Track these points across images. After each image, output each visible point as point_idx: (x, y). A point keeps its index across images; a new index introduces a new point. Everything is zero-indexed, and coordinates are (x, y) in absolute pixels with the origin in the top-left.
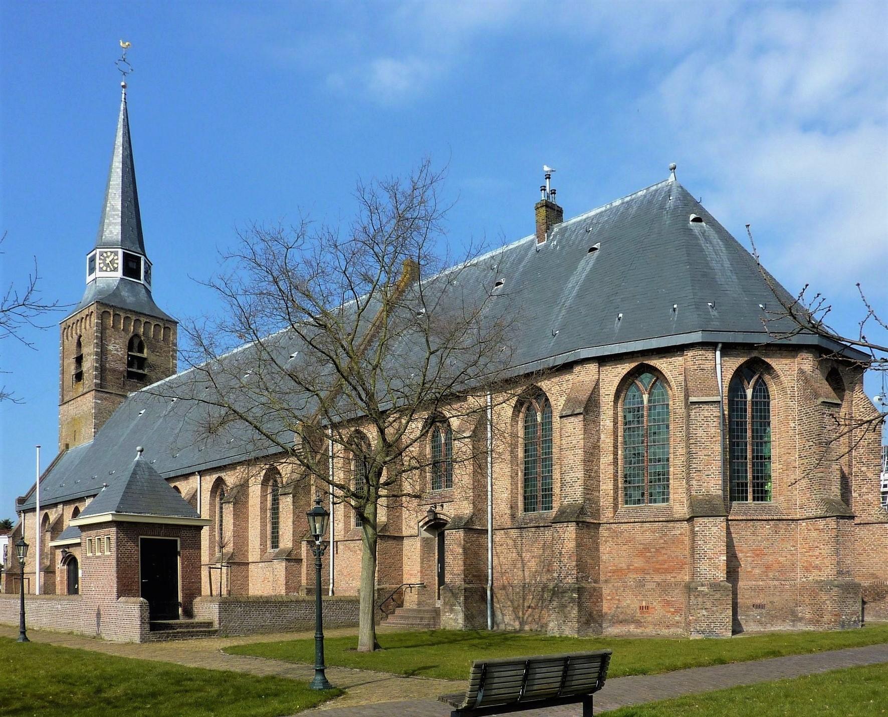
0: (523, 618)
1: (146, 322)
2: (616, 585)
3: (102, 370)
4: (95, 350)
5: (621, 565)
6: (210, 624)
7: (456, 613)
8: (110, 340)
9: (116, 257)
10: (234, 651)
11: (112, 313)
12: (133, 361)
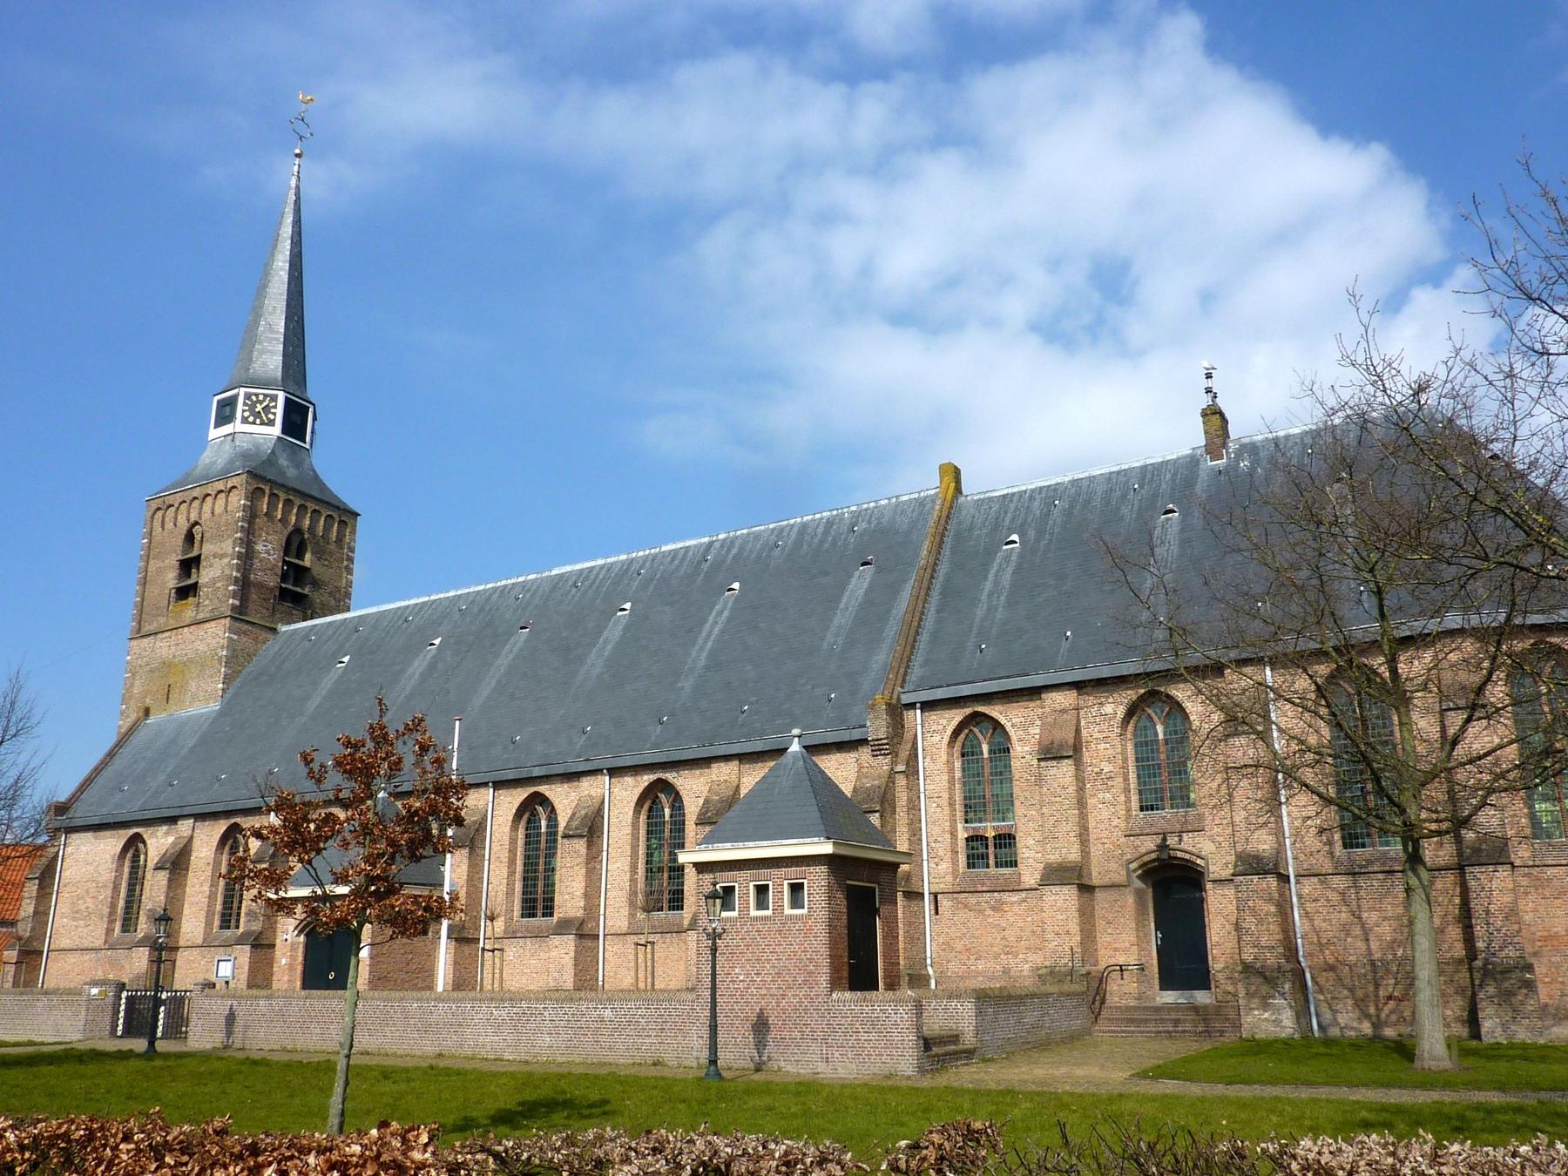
0: (1378, 1016)
1: (315, 511)
2: (1553, 959)
3: (245, 585)
4: (237, 549)
5: (1555, 929)
6: (955, 1038)
7: (1278, 1010)
8: (260, 536)
9: (273, 404)
11: (267, 492)
12: (295, 573)
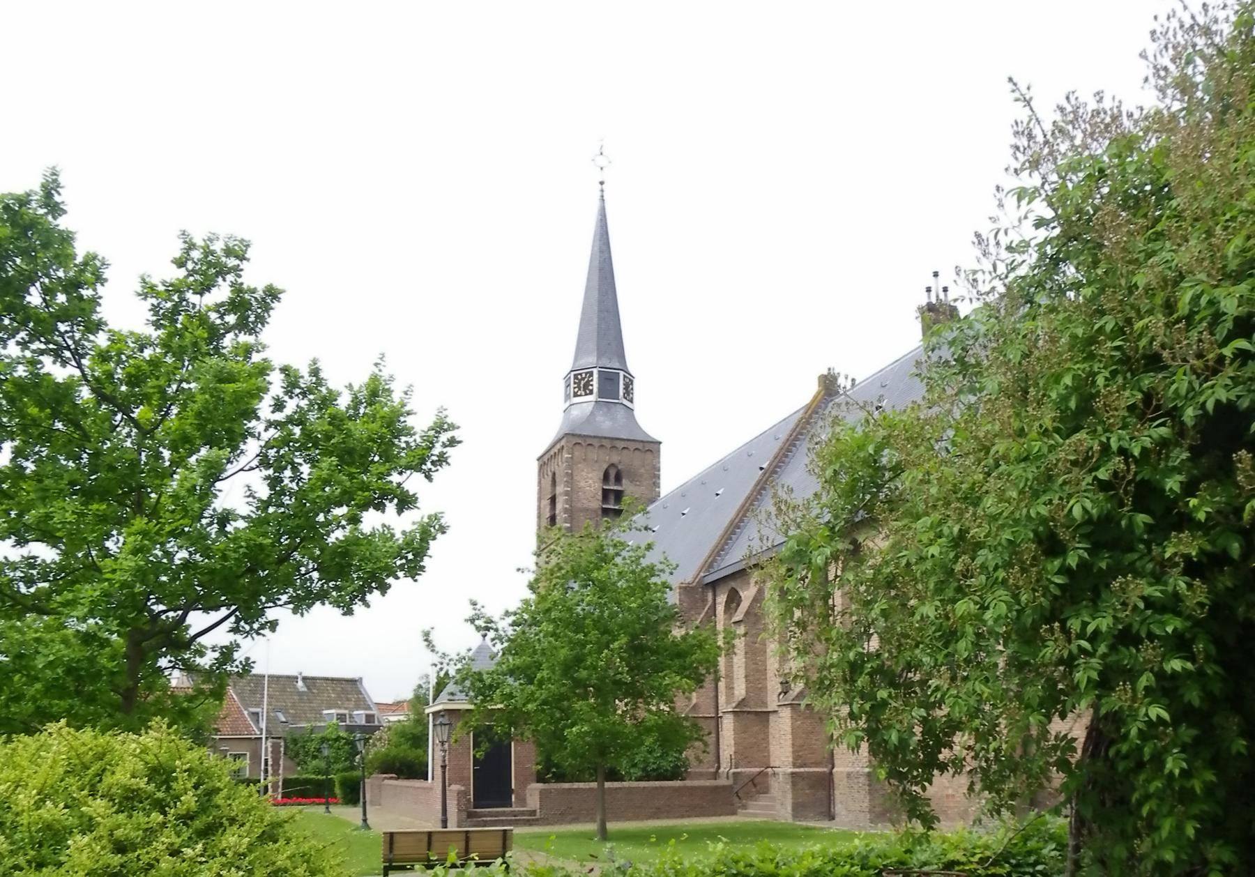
3: (571, 512)
6: (533, 813)
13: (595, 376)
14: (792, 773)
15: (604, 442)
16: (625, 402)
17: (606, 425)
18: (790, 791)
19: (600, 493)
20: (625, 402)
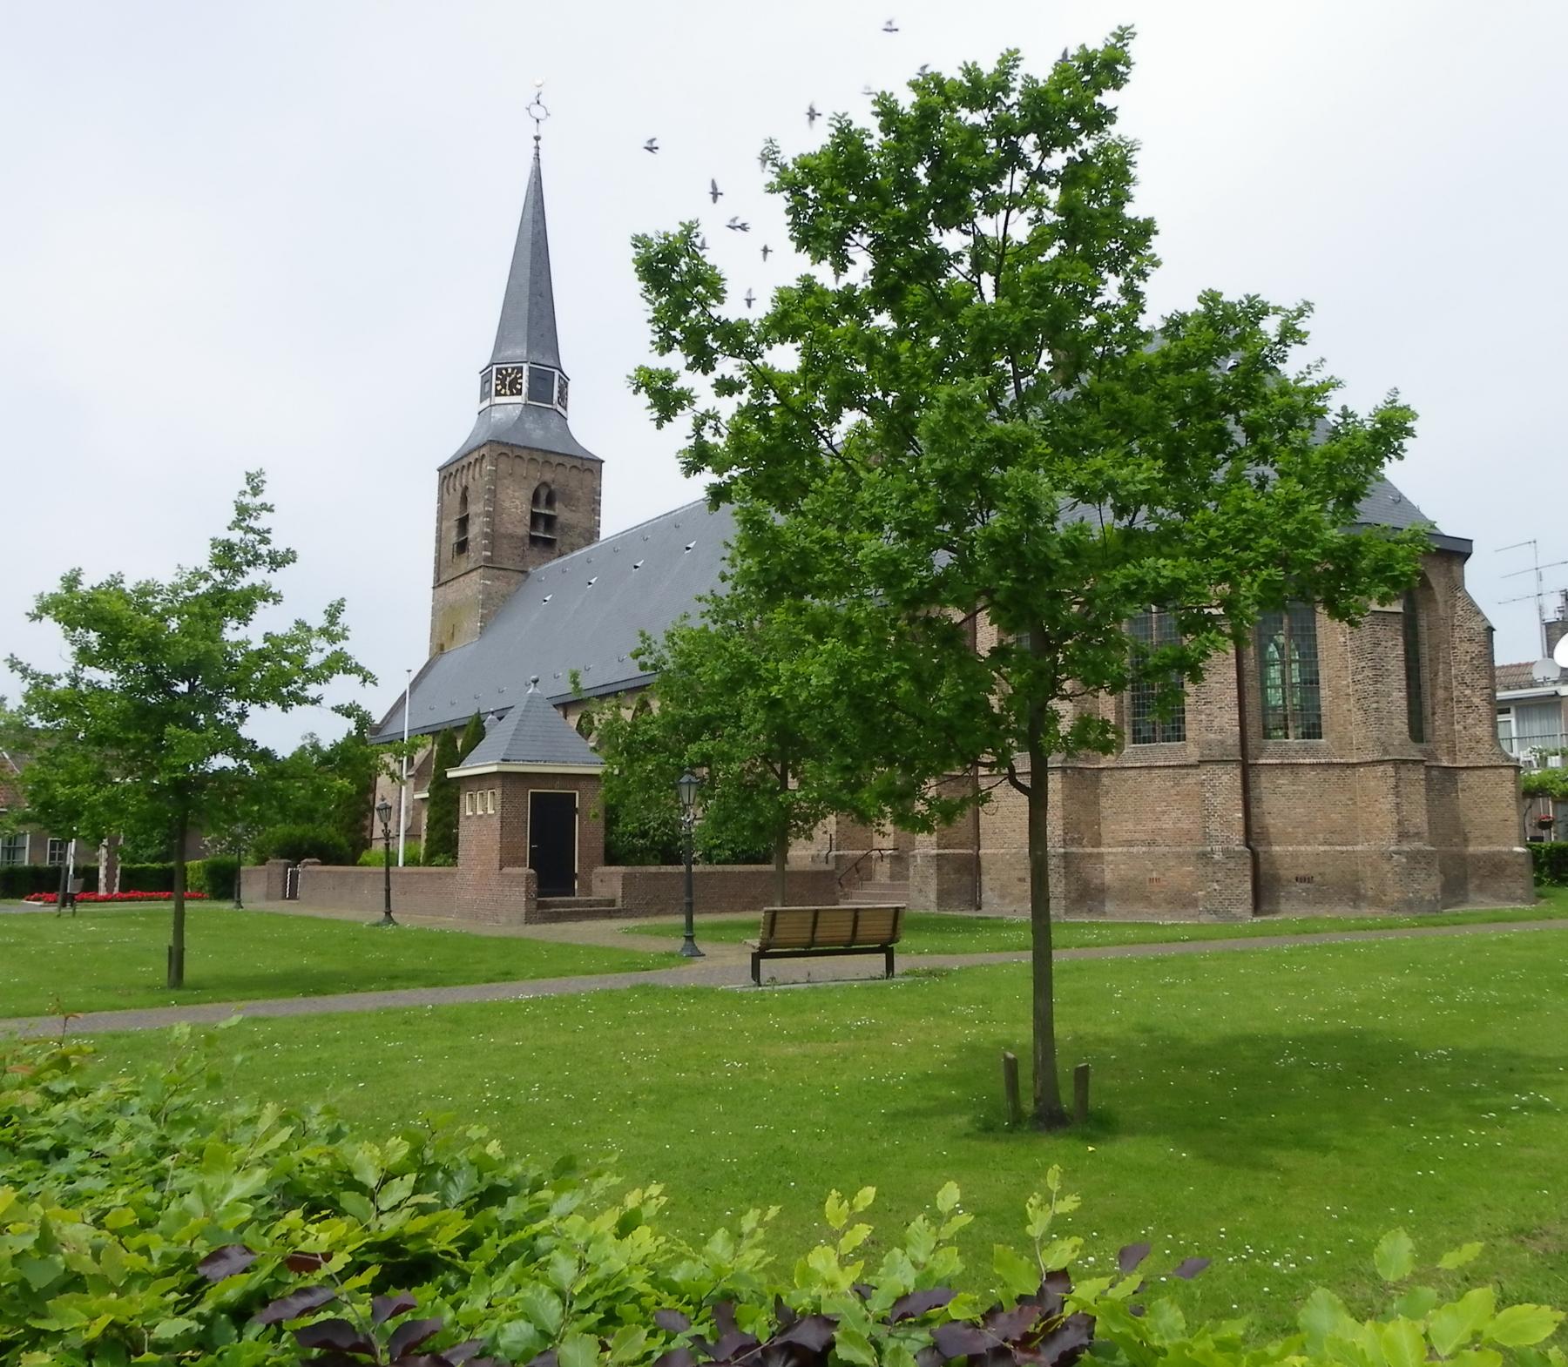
3: (493, 538)
6: (612, 902)
10: (628, 931)
13: (525, 373)
14: (938, 855)
15: (525, 454)
16: (560, 409)
17: (537, 435)
18: (935, 876)
19: (528, 517)
20: (560, 409)
